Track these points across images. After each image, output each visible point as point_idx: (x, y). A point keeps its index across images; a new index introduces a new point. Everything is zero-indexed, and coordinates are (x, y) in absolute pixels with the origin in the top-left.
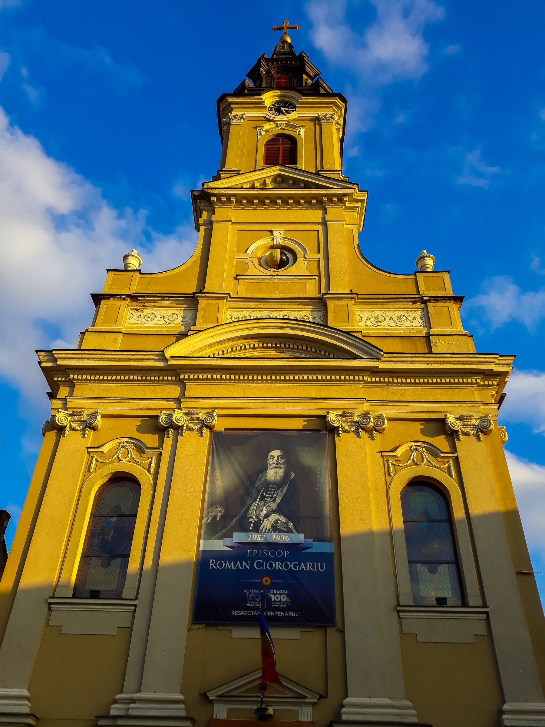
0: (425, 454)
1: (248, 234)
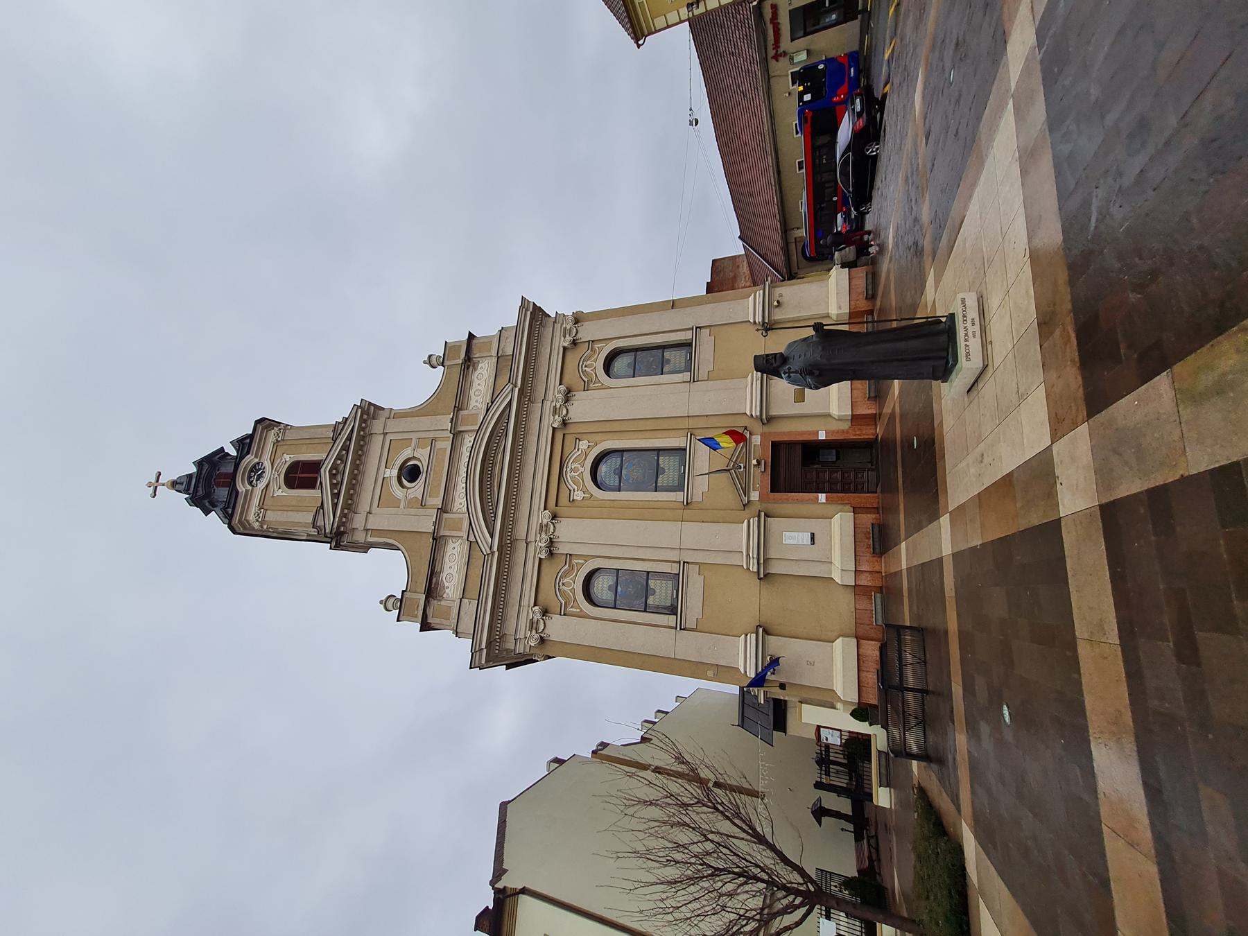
1: (384, 499)
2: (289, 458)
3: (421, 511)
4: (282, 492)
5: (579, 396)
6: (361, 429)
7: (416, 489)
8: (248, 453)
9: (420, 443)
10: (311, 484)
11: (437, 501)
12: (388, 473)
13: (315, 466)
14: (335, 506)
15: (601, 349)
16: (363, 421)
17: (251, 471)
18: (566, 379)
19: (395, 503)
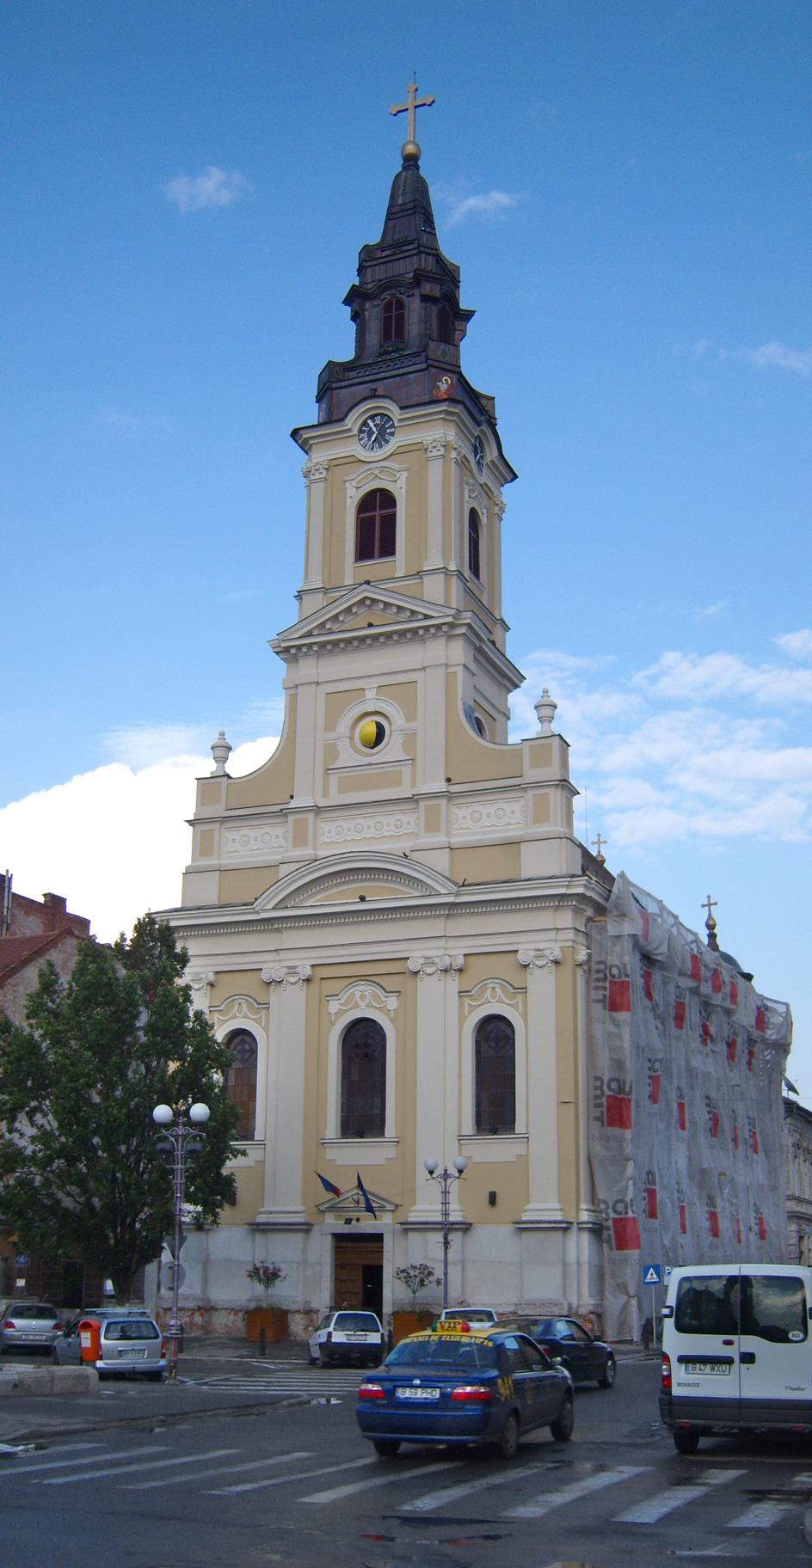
0: (499, 991)
2: (399, 490)
3: (419, 764)
4: (353, 497)
5: (453, 984)
6: (427, 628)
7: (349, 756)
8: (402, 408)
9: (410, 740)
10: (365, 551)
11: (336, 798)
12: (370, 694)
13: (389, 549)
14: (309, 634)
15: (515, 1006)
16: (438, 627)
17: (383, 415)
18: (472, 960)
19: (330, 725)
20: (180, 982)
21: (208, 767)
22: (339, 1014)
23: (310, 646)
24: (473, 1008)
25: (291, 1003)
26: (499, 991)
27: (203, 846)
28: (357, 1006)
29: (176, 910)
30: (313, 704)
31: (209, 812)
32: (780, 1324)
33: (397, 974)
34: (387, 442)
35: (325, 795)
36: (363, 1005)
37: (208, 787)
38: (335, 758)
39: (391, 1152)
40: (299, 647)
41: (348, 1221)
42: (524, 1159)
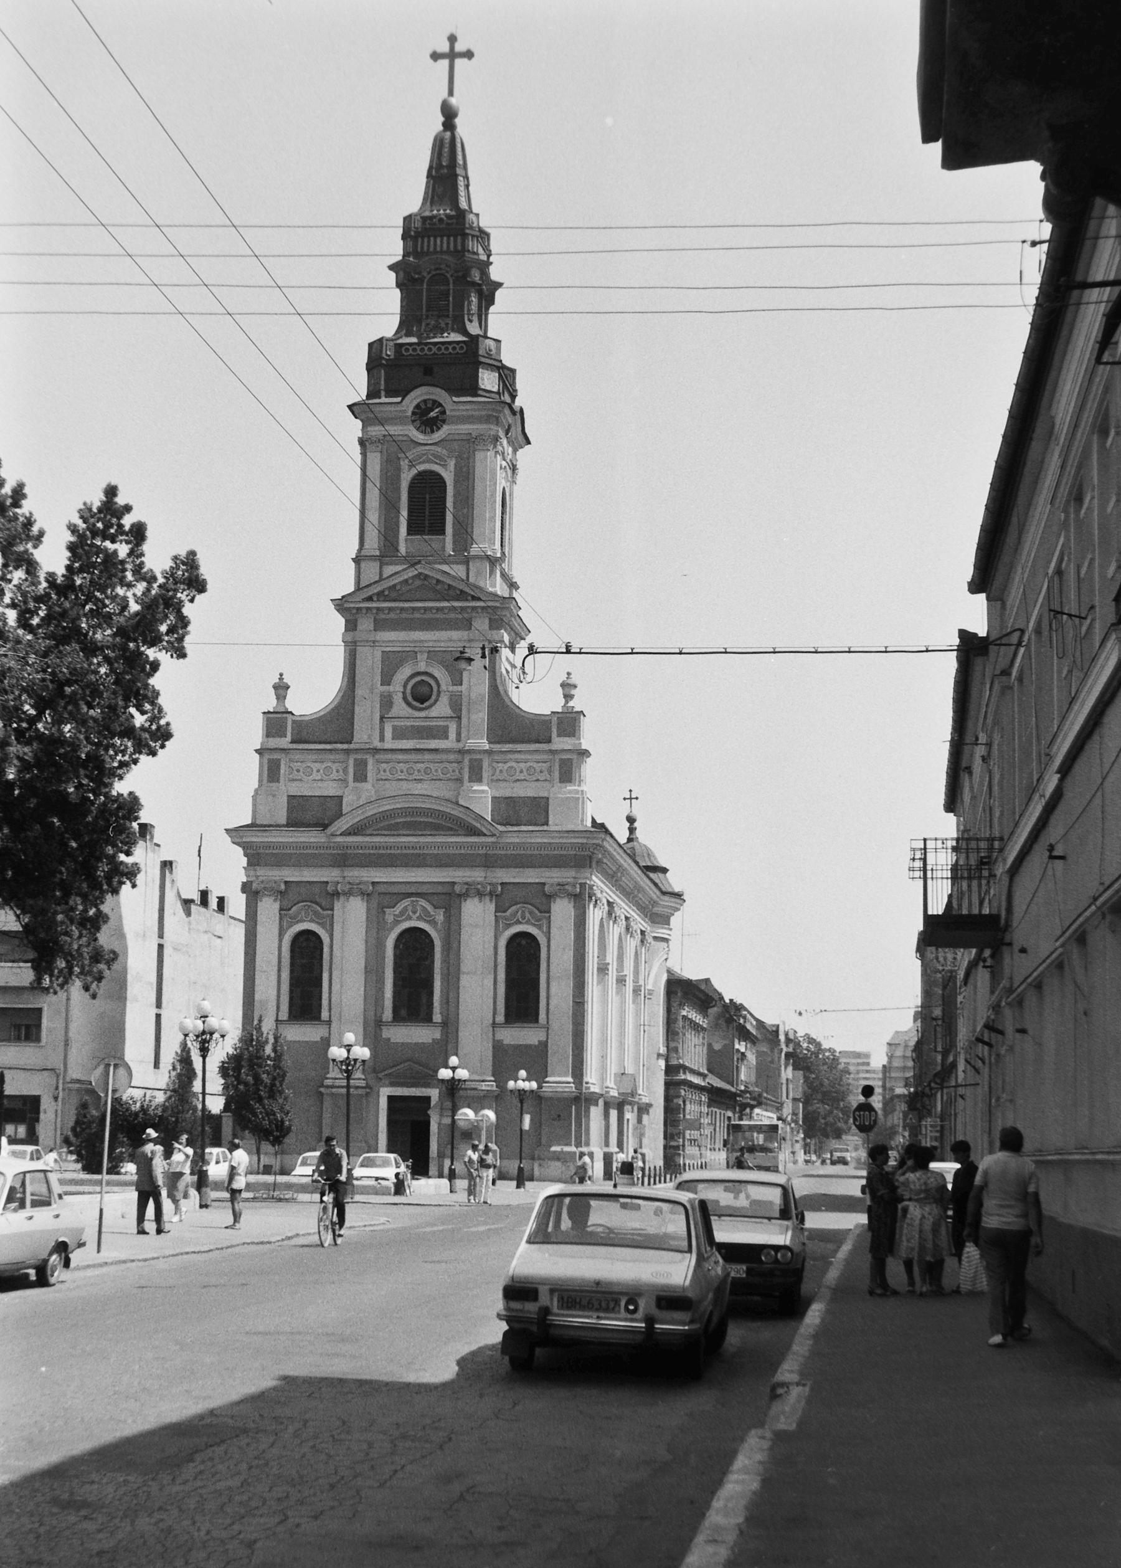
19: (386, 680)
20: (121, 788)
21: (271, 704)
22: (397, 922)
23: (368, 609)
24: (508, 926)
25: (352, 915)
26: (527, 915)
27: (271, 772)
28: (410, 918)
29: (247, 826)
30: (370, 661)
31: (274, 742)
32: (997, 584)
33: (449, 899)
34: (438, 429)
35: (382, 739)
36: (414, 917)
37: (275, 722)
38: (388, 712)
39: (437, 1034)
40: (359, 609)
41: (615, 1186)
42: (544, 1045)
